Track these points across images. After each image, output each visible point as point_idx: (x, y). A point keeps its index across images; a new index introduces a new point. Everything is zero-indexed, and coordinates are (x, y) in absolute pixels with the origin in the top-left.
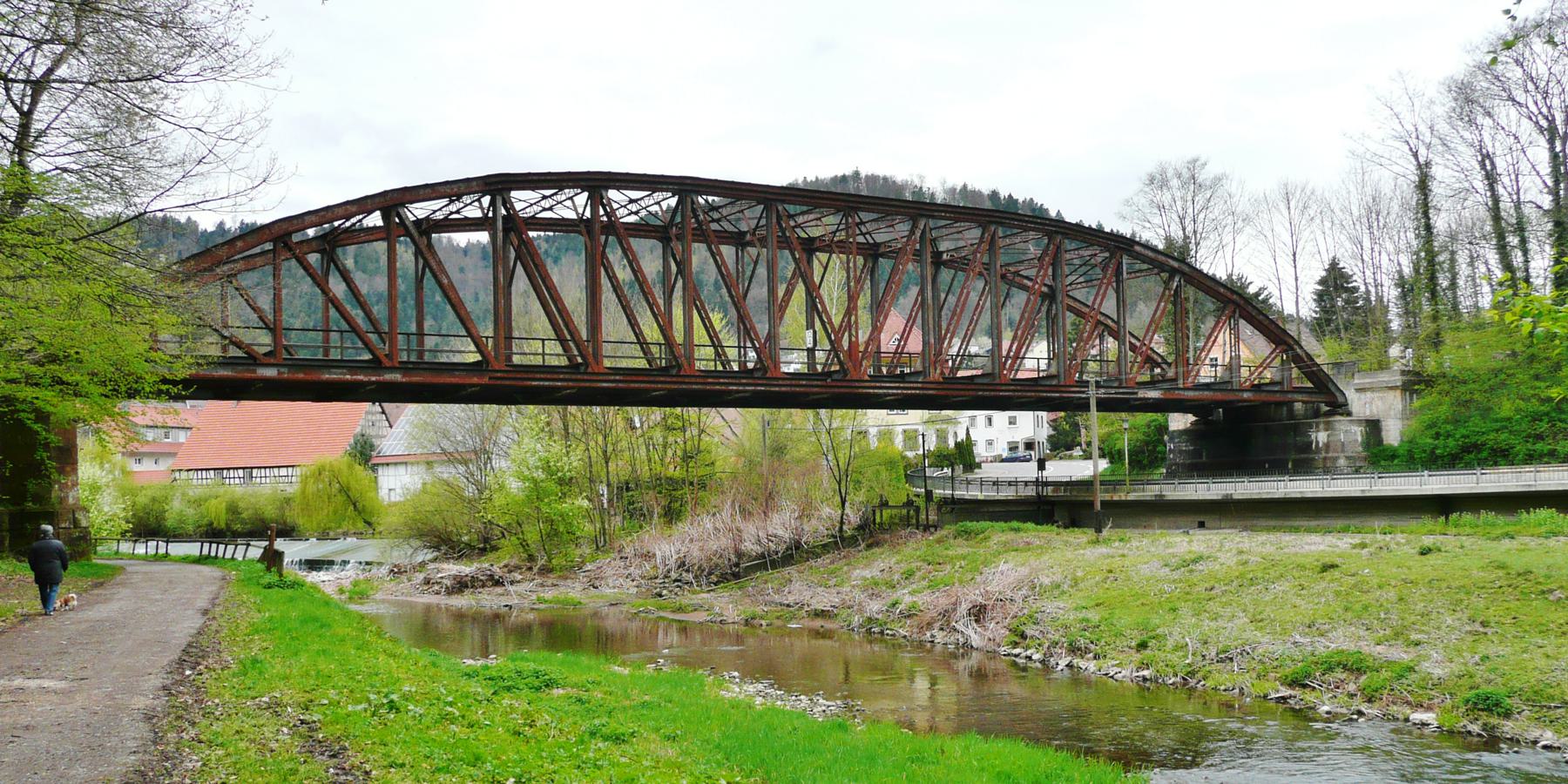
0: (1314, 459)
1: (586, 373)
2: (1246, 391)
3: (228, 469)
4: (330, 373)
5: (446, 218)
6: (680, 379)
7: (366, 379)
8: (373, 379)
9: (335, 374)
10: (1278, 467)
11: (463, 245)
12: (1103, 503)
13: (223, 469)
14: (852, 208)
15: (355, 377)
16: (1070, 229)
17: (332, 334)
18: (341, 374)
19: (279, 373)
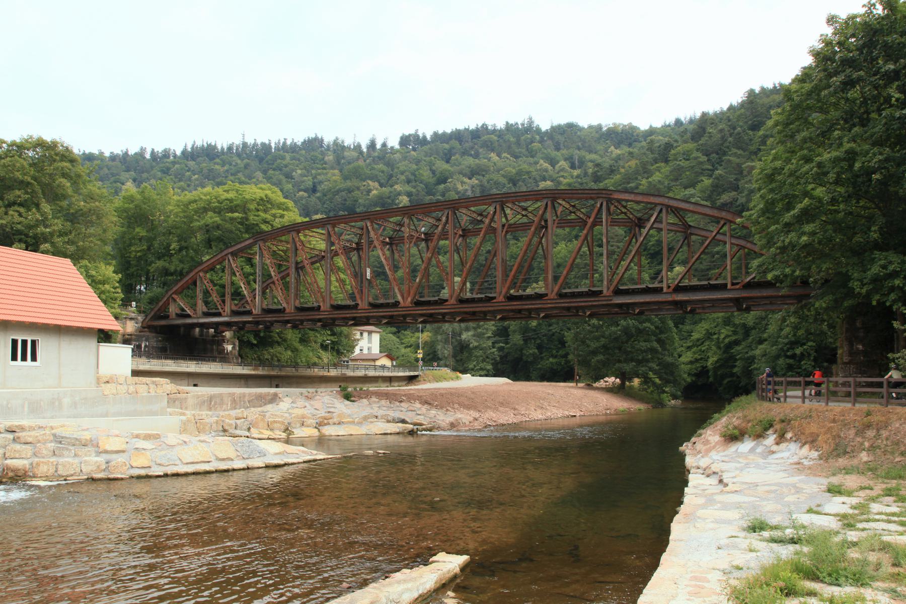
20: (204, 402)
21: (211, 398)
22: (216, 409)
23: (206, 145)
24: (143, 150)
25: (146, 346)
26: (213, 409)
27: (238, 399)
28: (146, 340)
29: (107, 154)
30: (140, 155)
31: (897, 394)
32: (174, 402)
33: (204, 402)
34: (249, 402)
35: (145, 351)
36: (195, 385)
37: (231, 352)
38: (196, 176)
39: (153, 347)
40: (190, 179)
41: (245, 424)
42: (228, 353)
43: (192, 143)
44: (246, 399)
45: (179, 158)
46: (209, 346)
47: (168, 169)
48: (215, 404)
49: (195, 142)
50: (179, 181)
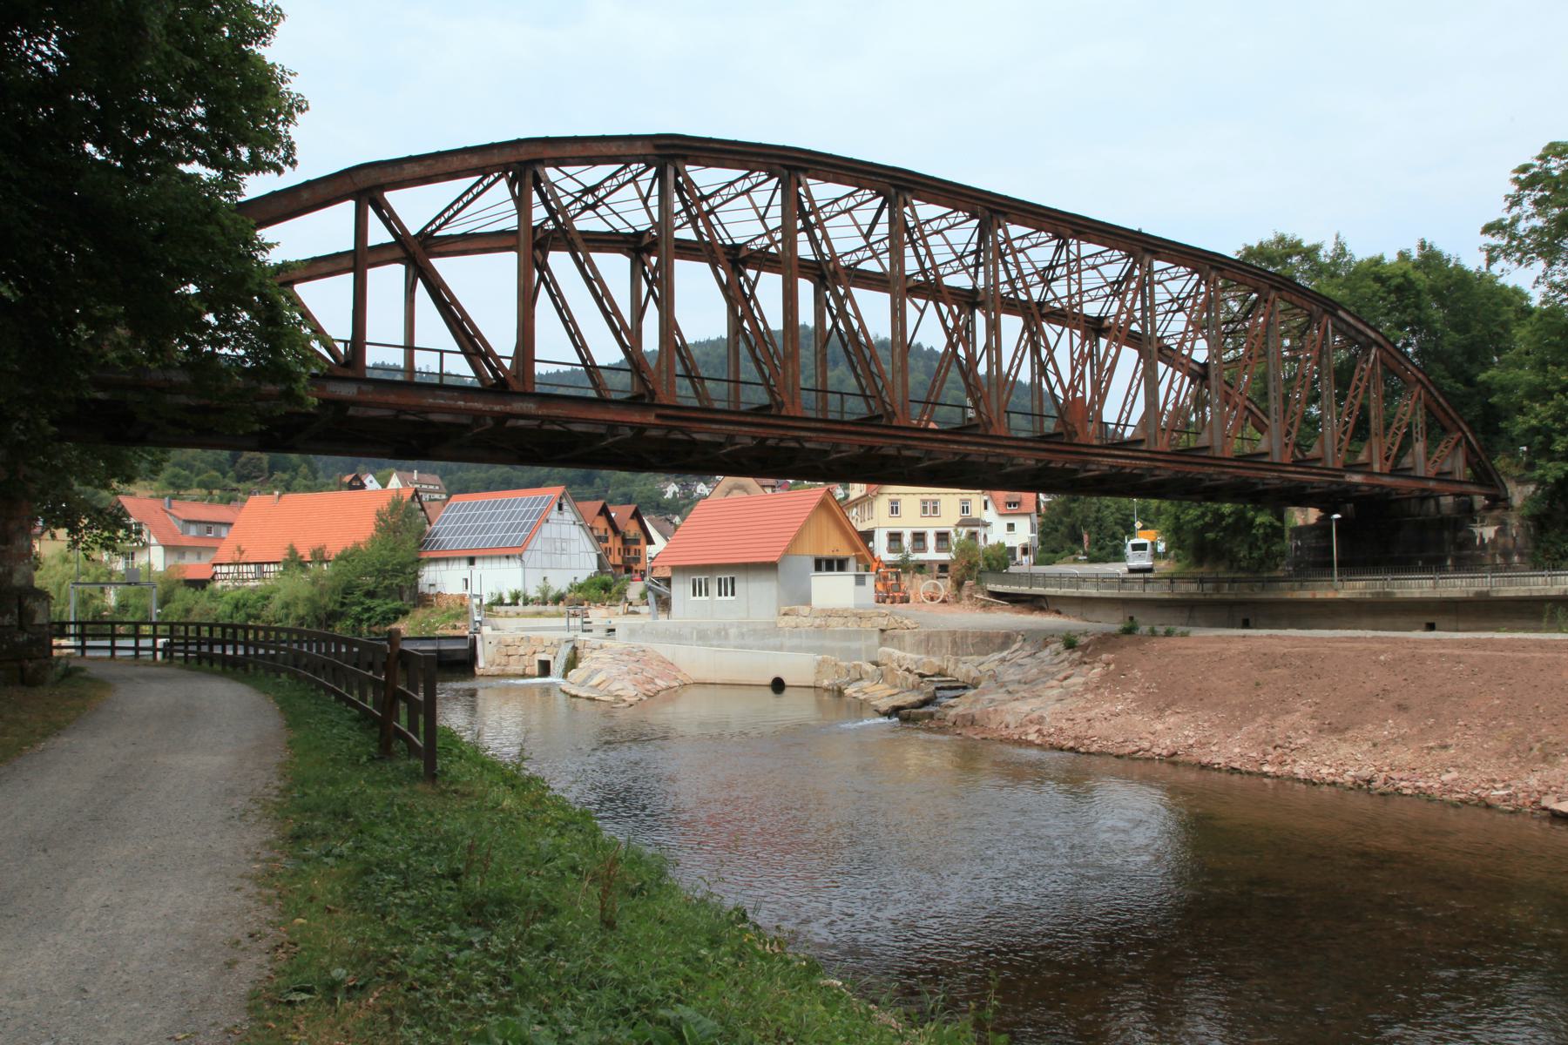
0: (1480, 557)
1: (886, 427)
2: (1431, 479)
3: (269, 563)
4: (435, 397)
5: (627, 165)
6: (892, 432)
7: (487, 408)
8: (497, 408)
9: (442, 397)
10: (1434, 565)
11: (196, 163)
12: (939, 550)
13: (263, 563)
14: (995, 211)
15: (470, 404)
16: (1230, 265)
17: (811, 384)
18: (451, 398)
19: (360, 392)
36: (1431, 627)
37: (1493, 542)
42: (1483, 546)
44: (969, 641)
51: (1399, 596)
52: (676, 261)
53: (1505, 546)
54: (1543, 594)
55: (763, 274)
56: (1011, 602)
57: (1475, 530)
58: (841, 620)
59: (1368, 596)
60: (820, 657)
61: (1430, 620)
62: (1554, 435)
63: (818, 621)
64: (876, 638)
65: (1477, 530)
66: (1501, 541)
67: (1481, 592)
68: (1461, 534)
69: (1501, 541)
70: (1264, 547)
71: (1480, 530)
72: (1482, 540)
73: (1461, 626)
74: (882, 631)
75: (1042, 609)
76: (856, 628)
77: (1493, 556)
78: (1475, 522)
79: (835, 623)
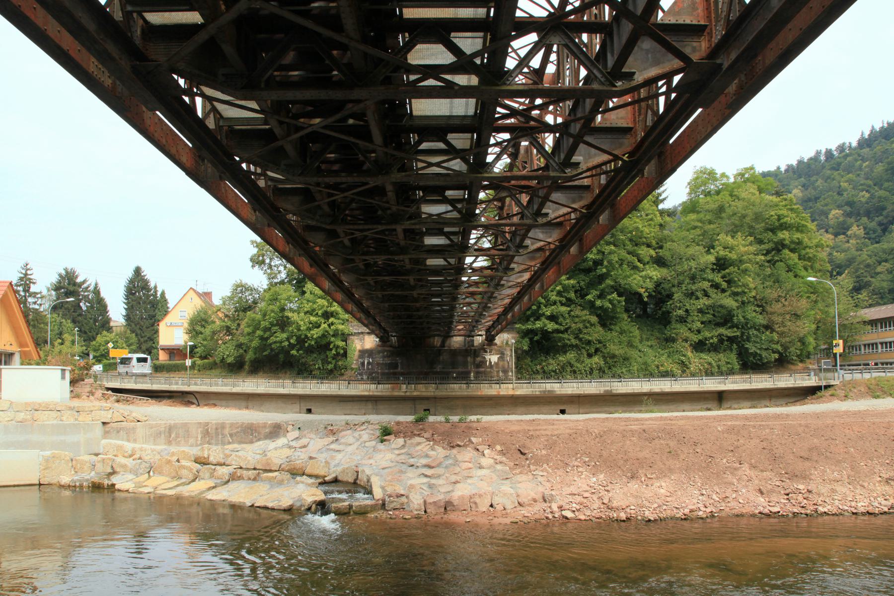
0: (491, 372)
20: (160, 433)
21: (170, 429)
22: (178, 444)
23: (886, 125)
24: (818, 153)
25: (369, 363)
26: (174, 443)
27: (214, 431)
28: (369, 357)
29: (783, 169)
30: (815, 159)
31: (458, 373)
32: (118, 432)
33: (160, 433)
34: (231, 435)
35: (368, 369)
36: (563, 412)
37: (497, 364)
38: (867, 163)
39: (378, 364)
40: (860, 169)
41: (143, 466)
42: (491, 366)
43: (870, 128)
44: (227, 431)
45: (855, 149)
46: (460, 358)
47: (839, 164)
48: (177, 436)
49: (873, 127)
50: (848, 174)
51: (559, 393)
52: (203, 21)
53: (503, 367)
54: (640, 391)
55: (519, 5)
56: (151, 397)
57: (486, 357)
58: (54, 414)
59: (537, 393)
60: (48, 453)
61: (562, 408)
62: (542, 306)
63: (21, 416)
64: (99, 430)
65: (488, 357)
66: (501, 363)
67: (608, 390)
68: (478, 359)
69: (501, 363)
70: (334, 362)
71: (489, 357)
72: (490, 362)
73: (581, 411)
74: (104, 423)
75: (189, 403)
76: (72, 421)
77: (498, 372)
78: (486, 352)
79: (45, 418)
